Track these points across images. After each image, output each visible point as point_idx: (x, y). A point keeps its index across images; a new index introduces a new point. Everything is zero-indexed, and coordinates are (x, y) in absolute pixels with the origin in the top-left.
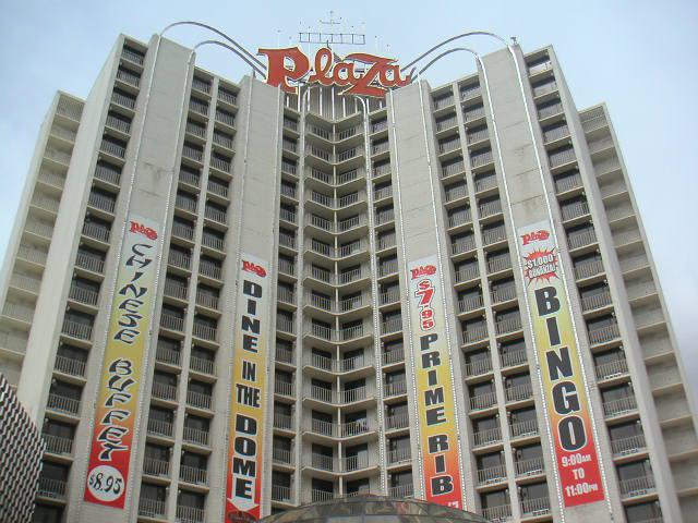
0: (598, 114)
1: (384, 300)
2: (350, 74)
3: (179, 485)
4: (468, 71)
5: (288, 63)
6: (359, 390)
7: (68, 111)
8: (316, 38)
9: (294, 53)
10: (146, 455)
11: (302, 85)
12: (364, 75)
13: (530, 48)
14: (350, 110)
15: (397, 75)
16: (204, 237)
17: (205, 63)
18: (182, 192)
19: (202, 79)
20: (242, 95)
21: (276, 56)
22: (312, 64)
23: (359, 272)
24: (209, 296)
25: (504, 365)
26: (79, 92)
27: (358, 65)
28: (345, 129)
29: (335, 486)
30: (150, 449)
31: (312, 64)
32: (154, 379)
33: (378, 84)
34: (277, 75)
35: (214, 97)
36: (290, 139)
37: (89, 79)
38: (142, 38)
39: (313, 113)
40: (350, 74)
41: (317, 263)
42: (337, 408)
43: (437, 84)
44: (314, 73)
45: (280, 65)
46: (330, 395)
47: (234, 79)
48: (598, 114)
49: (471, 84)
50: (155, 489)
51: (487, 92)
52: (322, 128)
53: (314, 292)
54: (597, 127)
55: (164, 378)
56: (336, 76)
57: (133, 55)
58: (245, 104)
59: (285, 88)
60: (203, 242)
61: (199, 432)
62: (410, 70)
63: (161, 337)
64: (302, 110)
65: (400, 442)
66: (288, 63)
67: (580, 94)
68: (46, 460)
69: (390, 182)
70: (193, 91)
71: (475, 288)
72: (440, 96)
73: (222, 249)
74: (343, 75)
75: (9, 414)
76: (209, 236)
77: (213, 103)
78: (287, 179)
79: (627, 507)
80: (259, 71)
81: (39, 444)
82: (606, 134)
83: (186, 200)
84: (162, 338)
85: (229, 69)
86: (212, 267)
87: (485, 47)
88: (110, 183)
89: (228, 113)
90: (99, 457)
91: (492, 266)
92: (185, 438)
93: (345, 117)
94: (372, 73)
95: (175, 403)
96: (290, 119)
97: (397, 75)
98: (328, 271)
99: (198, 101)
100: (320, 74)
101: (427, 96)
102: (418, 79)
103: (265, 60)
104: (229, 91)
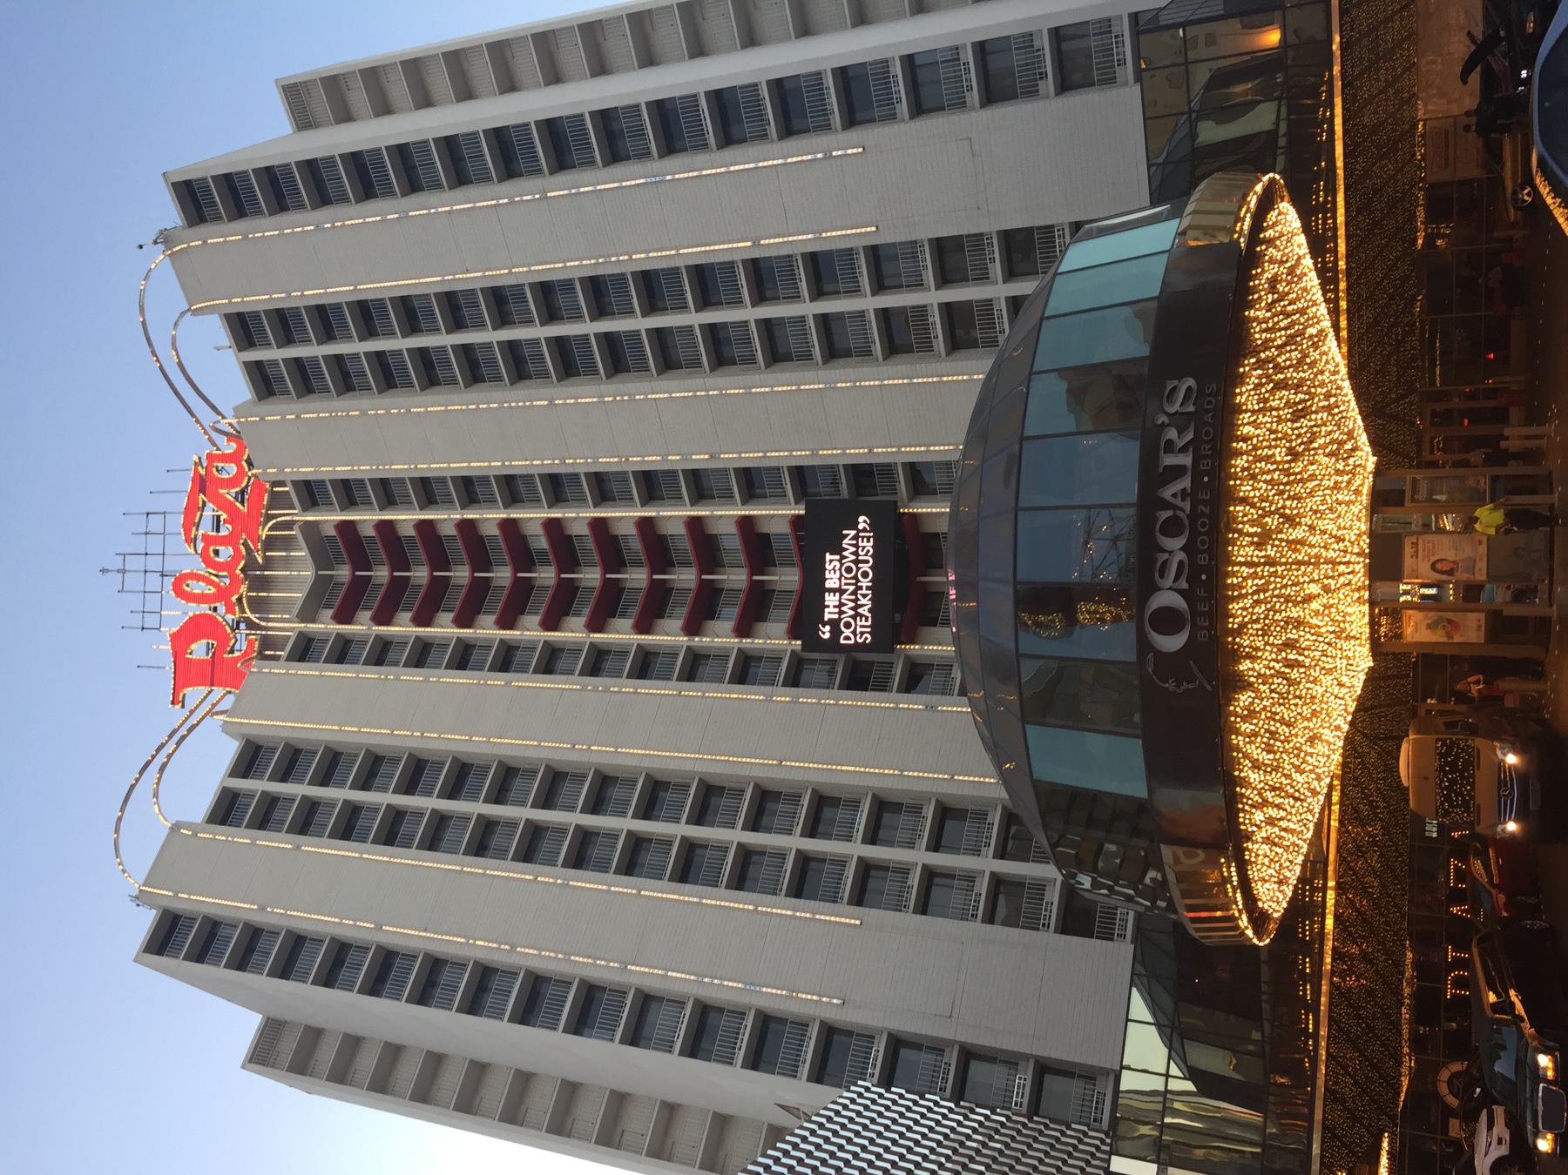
0: (297, 96)
4: (216, 331)
5: (199, 650)
7: (285, 1052)
8: (153, 602)
9: (181, 640)
11: (242, 626)
12: (224, 516)
13: (170, 214)
14: (287, 543)
15: (226, 458)
19: (226, 810)
21: (186, 673)
22: (204, 608)
25: (631, 312)
26: (246, 1025)
27: (206, 528)
30: (747, 884)
31: (204, 608)
32: (695, 883)
33: (243, 492)
34: (215, 672)
36: (342, 652)
37: (218, 1020)
38: (146, 920)
39: (296, 610)
40: (225, 541)
43: (240, 389)
44: (222, 608)
45: (200, 664)
47: (230, 749)
48: (297, 96)
49: (244, 329)
50: (935, 891)
51: (258, 300)
54: (310, 100)
55: (752, 872)
56: (228, 566)
57: (179, 938)
58: (278, 726)
59: (246, 659)
60: (571, 808)
61: (725, 801)
62: (215, 435)
63: (923, 908)
64: (286, 626)
66: (199, 650)
67: (261, 133)
68: (887, 1081)
70: (375, 841)
72: (264, 381)
73: (534, 772)
74: (226, 553)
75: (809, 1154)
76: (561, 800)
77: (274, 788)
79: (851, 121)
80: (214, 705)
81: (860, 1095)
82: (334, 84)
83: (496, 840)
85: (208, 764)
86: (518, 783)
87: (168, 294)
89: (292, 761)
90: (1445, 1075)
92: (848, 838)
93: (302, 553)
94: (221, 503)
96: (304, 650)
97: (226, 458)
99: (266, 816)
100: (222, 594)
101: (265, 407)
102: (234, 421)
103: (194, 694)
104: (250, 759)
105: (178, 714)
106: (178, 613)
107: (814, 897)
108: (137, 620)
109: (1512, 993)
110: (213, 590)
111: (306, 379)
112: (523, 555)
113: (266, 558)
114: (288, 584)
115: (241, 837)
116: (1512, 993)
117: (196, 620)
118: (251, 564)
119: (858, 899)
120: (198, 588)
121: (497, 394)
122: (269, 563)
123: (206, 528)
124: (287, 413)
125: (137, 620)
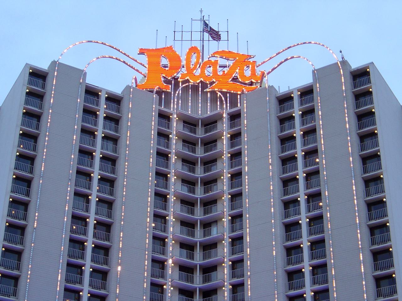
1: (232, 145)
2: (215, 72)
3: (89, 291)
4: (306, 80)
6: (213, 274)
9: (168, 51)
10: (69, 247)
13: (355, 64)
16: (101, 165)
17: (92, 80)
18: (84, 131)
19: (92, 93)
20: (124, 104)
22: (184, 63)
23: (216, 145)
24: (110, 144)
25: (309, 211)
27: (222, 61)
28: (211, 123)
29: (196, 164)
30: (72, 244)
31: (184, 63)
35: (102, 109)
38: (44, 65)
41: (187, 120)
42: (198, 178)
46: (195, 149)
47: (117, 89)
49: (307, 93)
51: (318, 102)
52: (189, 123)
53: (184, 141)
58: (128, 115)
64: (174, 109)
65: (238, 242)
69: (242, 193)
71: (292, 138)
72: (285, 100)
77: (102, 111)
78: (160, 151)
84: (72, 241)
88: (33, 130)
89: (113, 120)
91: (305, 122)
94: (232, 68)
95: (86, 238)
96: (164, 117)
98: (195, 125)
104: (114, 100)
105: (134, 53)
106: (182, 50)
107: (67, 271)
108: (178, 29)
109: (246, 171)
110: (192, 67)
111: (285, 120)
112: (207, 225)
113: (207, 92)
114: (195, 107)
115: (80, 101)
116: (246, 171)
117: (178, 58)
118: (204, 85)
119: (67, 290)
120: (194, 60)
121: (278, 216)
122: (204, 94)
123: (222, 61)
124: (272, 111)
125: (178, 29)
